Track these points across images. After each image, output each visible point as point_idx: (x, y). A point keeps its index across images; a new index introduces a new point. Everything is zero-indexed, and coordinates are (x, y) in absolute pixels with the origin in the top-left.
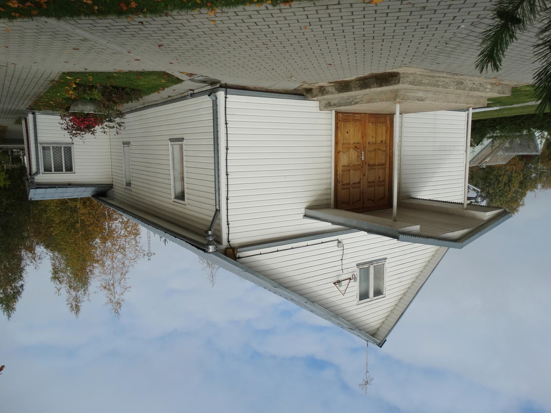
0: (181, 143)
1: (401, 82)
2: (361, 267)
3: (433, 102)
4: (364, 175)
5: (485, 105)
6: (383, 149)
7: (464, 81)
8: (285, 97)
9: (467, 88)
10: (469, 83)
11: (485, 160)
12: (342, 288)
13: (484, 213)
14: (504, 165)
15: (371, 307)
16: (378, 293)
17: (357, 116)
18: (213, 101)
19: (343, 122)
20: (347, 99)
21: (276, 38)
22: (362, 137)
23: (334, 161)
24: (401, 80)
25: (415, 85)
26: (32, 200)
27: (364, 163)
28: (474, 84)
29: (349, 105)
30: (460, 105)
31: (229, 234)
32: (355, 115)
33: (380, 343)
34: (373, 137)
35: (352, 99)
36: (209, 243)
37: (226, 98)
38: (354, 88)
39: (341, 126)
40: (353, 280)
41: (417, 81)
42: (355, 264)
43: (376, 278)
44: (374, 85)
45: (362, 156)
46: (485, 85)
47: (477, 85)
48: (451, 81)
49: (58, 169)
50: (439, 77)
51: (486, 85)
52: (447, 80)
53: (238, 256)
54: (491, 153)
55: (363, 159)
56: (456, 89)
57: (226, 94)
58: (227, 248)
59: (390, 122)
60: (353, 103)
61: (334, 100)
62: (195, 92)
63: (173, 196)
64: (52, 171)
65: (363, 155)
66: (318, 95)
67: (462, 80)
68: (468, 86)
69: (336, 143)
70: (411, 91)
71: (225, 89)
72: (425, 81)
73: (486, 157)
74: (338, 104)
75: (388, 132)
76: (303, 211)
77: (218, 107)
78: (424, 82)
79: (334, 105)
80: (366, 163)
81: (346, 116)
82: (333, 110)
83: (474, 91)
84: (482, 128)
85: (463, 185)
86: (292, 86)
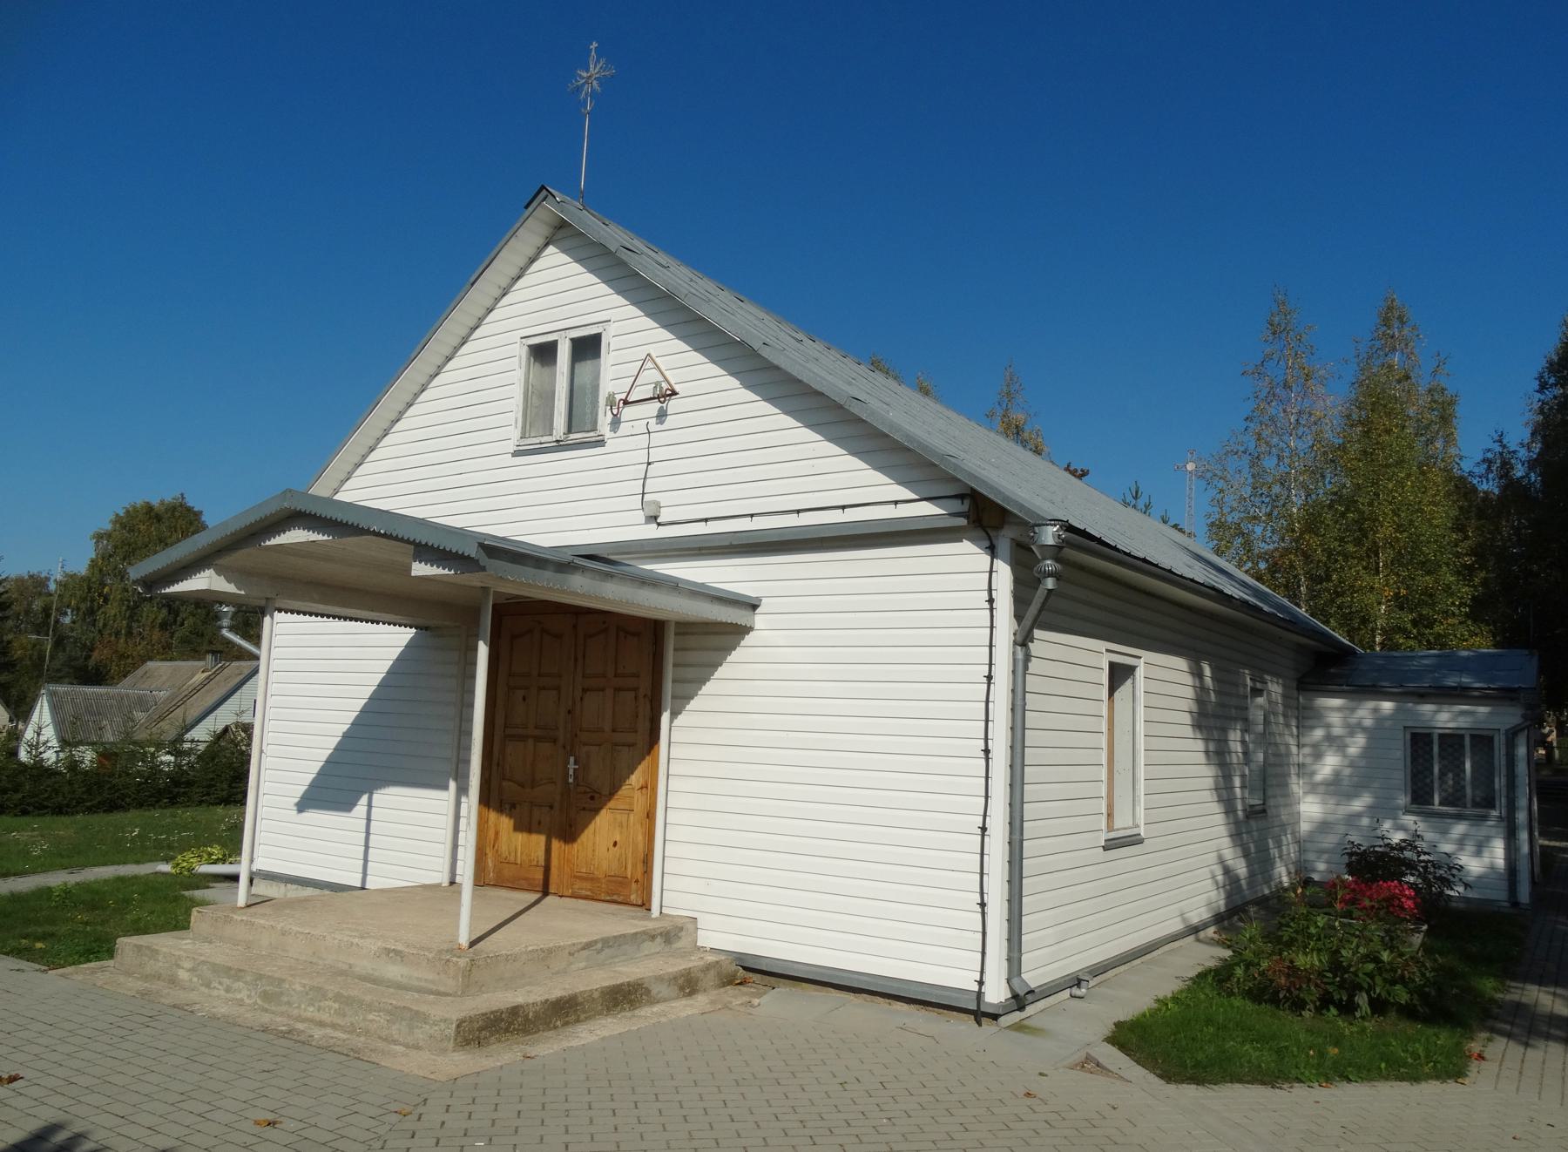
0: (1113, 835)
1: (454, 1026)
2: (592, 434)
3: (356, 940)
4: (569, 712)
5: (199, 912)
6: (510, 783)
7: (259, 1002)
8: (801, 966)
9: (249, 978)
10: (243, 995)
11: (207, 678)
12: (651, 375)
13: (213, 588)
14: (151, 659)
15: (567, 312)
16: (543, 353)
17: (586, 890)
18: (1020, 974)
19: (626, 877)
20: (616, 956)
21: (815, 1139)
22: (571, 826)
23: (660, 765)
24: (451, 1031)
25: (410, 1010)
26: (1526, 652)
27: (568, 748)
28: (228, 990)
29: (608, 938)
30: (272, 923)
31: (991, 572)
32: (589, 893)
33: (544, 199)
34: (539, 823)
35: (602, 956)
36: (1057, 552)
37: (981, 983)
38: (594, 999)
39: (634, 866)
40: (618, 397)
41: (404, 1023)
42: (609, 447)
43: (549, 397)
44: (535, 1012)
45: (575, 769)
46: (195, 979)
47: (220, 983)
48: (299, 1007)
49: (1452, 741)
50: (334, 1026)
51: (191, 980)
52: (310, 1012)
53: (967, 502)
54: (189, 697)
55: (572, 759)
56: (284, 980)
57: (980, 994)
58: (999, 527)
59: (486, 862)
60: (599, 946)
61: (653, 951)
62: (1068, 990)
63: (1140, 673)
64: (1471, 735)
65: (571, 772)
66: (702, 971)
67: (266, 1006)
68: (246, 983)
69: (650, 816)
70: (423, 984)
71: (983, 1009)
72: (377, 1019)
73: (203, 684)
74: (644, 941)
75: (491, 834)
76: (759, 620)
77: (1005, 956)
78: (381, 1014)
79: (653, 938)
80: (564, 747)
81: (619, 895)
82: (656, 919)
83: (230, 969)
84: (212, 779)
85: (274, 653)
86: (773, 1003)
